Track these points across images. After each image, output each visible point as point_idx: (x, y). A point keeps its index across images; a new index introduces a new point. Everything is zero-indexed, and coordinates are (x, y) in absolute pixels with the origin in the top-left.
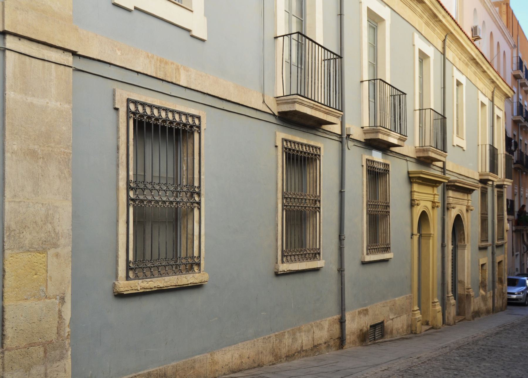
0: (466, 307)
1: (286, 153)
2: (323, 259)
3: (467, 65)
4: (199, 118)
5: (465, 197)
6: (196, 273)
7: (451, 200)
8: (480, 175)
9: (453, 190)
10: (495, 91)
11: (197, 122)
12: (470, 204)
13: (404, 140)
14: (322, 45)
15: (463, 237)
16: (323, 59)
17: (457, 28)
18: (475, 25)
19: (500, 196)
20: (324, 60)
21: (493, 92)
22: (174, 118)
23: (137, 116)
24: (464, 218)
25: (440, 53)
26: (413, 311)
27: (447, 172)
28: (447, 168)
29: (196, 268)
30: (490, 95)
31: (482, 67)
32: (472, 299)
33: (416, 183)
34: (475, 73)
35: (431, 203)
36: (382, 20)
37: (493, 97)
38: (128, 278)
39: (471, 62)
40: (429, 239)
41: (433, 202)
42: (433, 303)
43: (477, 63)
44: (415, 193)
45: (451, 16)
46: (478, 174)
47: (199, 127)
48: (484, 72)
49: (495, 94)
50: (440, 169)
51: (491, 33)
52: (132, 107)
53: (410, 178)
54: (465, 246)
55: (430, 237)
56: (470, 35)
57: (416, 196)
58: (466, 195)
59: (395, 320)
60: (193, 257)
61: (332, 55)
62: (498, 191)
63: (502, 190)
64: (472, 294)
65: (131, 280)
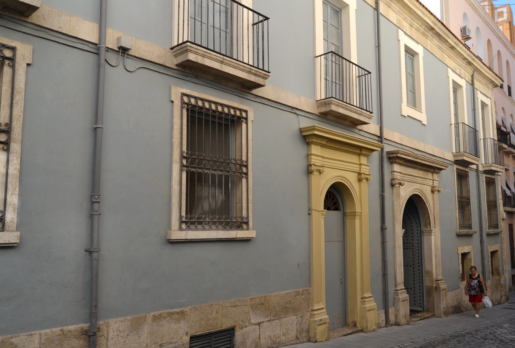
0: (436, 301)
1: (187, 110)
2: (253, 229)
3: (424, 34)
4: (246, 112)
5: (430, 176)
6: (244, 230)
7: (397, 176)
8: (454, 156)
9: (400, 164)
10: (475, 75)
11: (244, 115)
12: (435, 185)
13: (265, 78)
14: (252, 8)
15: (428, 221)
16: (357, 75)
17: (447, 32)
18: (463, 25)
19: (491, 183)
20: (359, 77)
21: (472, 76)
22: (223, 110)
23: (190, 106)
24: (427, 200)
25: (373, 9)
26: (313, 310)
27: (385, 141)
28: (385, 135)
29: (245, 226)
30: (469, 78)
31: (447, 41)
32: (442, 292)
33: (316, 144)
34: (440, 48)
35: (357, 174)
36: (461, 87)
37: (473, 81)
38: (180, 229)
39: (431, 33)
40: (355, 219)
41: (359, 174)
42: (362, 298)
43: (438, 35)
44: (313, 157)
45: (435, 16)
46: (451, 155)
47: (246, 119)
48: (452, 48)
49: (475, 77)
50: (376, 138)
51: (489, 41)
52: (186, 99)
53: (305, 137)
54: (430, 232)
55: (355, 215)
56: (459, 36)
57: (314, 160)
58: (430, 174)
59: (265, 325)
60: (242, 218)
61: (363, 71)
62: (486, 177)
63: (493, 177)
64: (443, 286)
65: (183, 230)
